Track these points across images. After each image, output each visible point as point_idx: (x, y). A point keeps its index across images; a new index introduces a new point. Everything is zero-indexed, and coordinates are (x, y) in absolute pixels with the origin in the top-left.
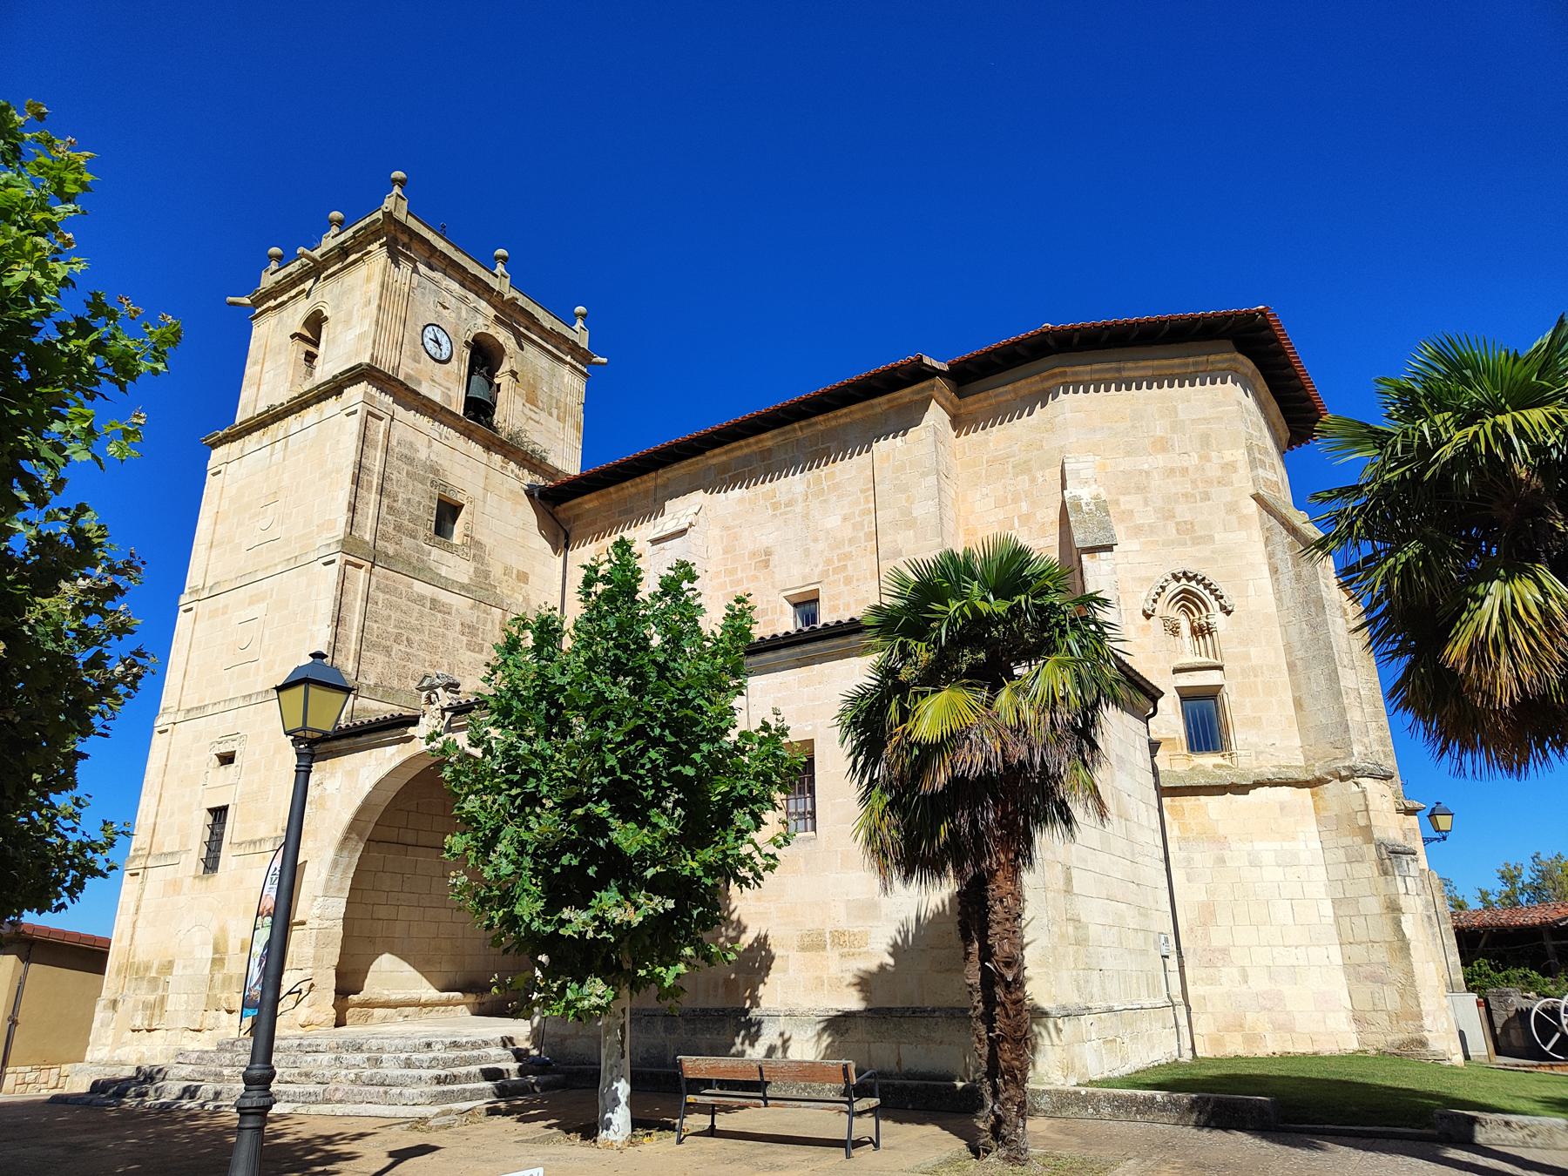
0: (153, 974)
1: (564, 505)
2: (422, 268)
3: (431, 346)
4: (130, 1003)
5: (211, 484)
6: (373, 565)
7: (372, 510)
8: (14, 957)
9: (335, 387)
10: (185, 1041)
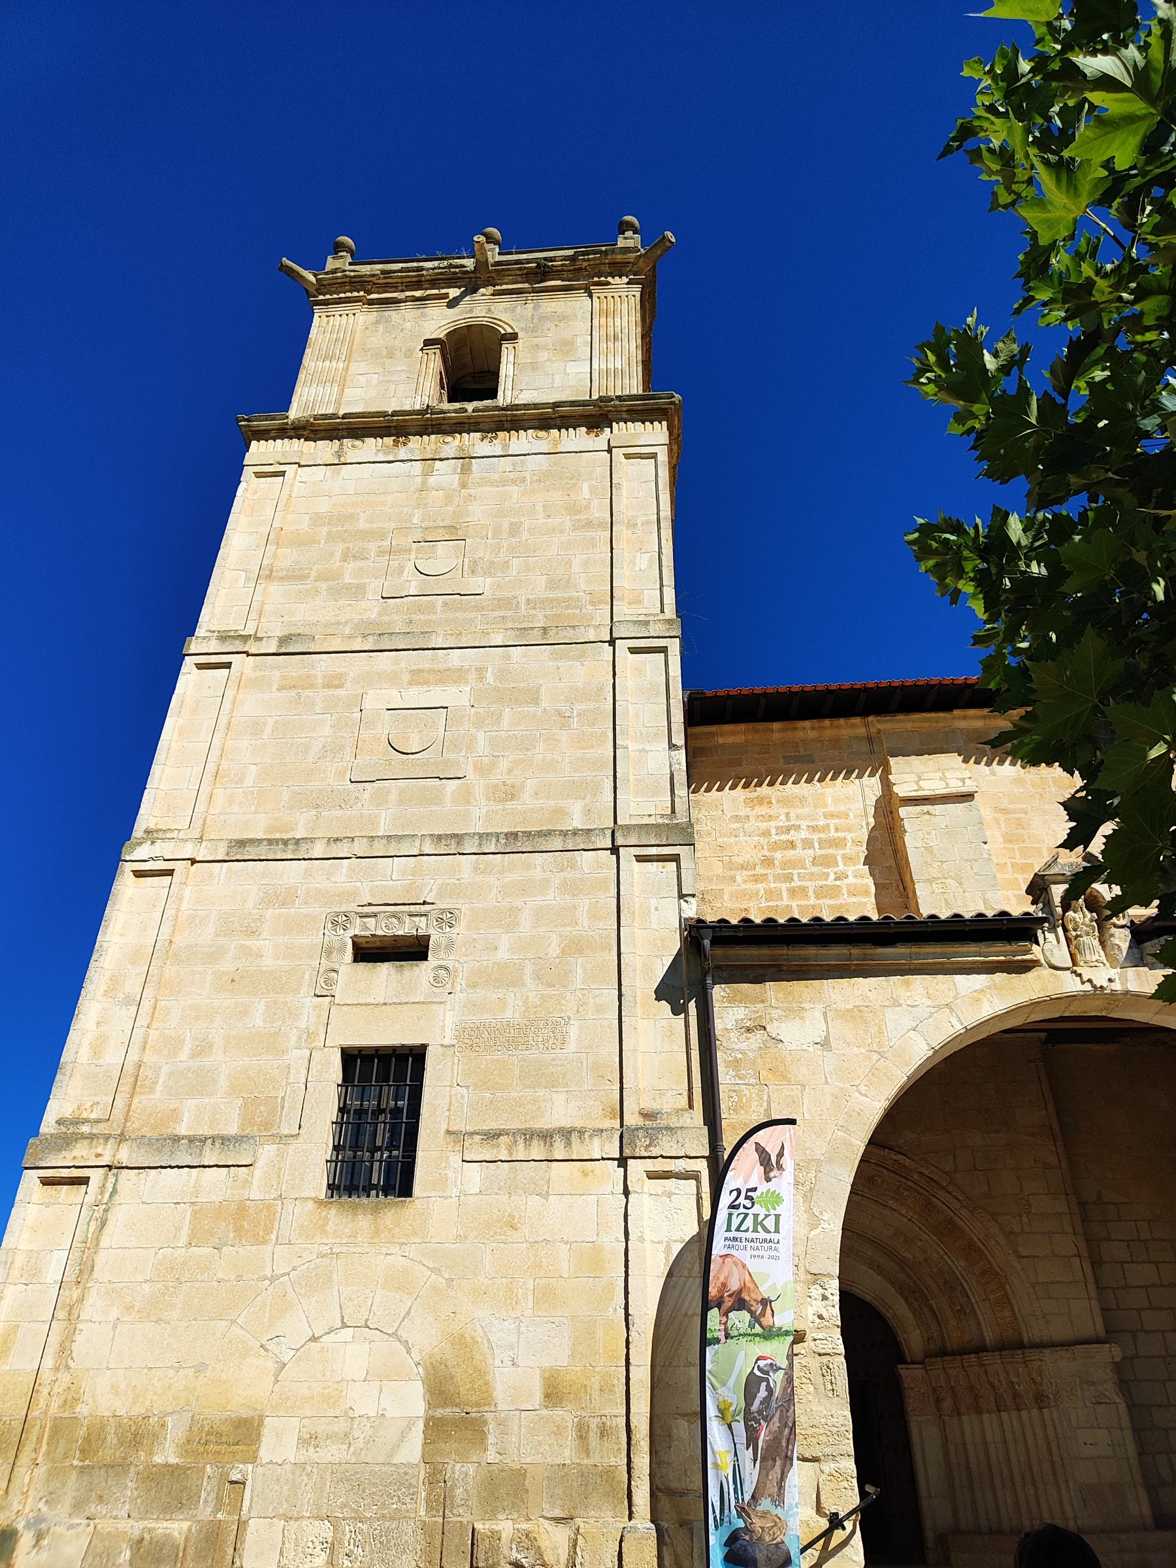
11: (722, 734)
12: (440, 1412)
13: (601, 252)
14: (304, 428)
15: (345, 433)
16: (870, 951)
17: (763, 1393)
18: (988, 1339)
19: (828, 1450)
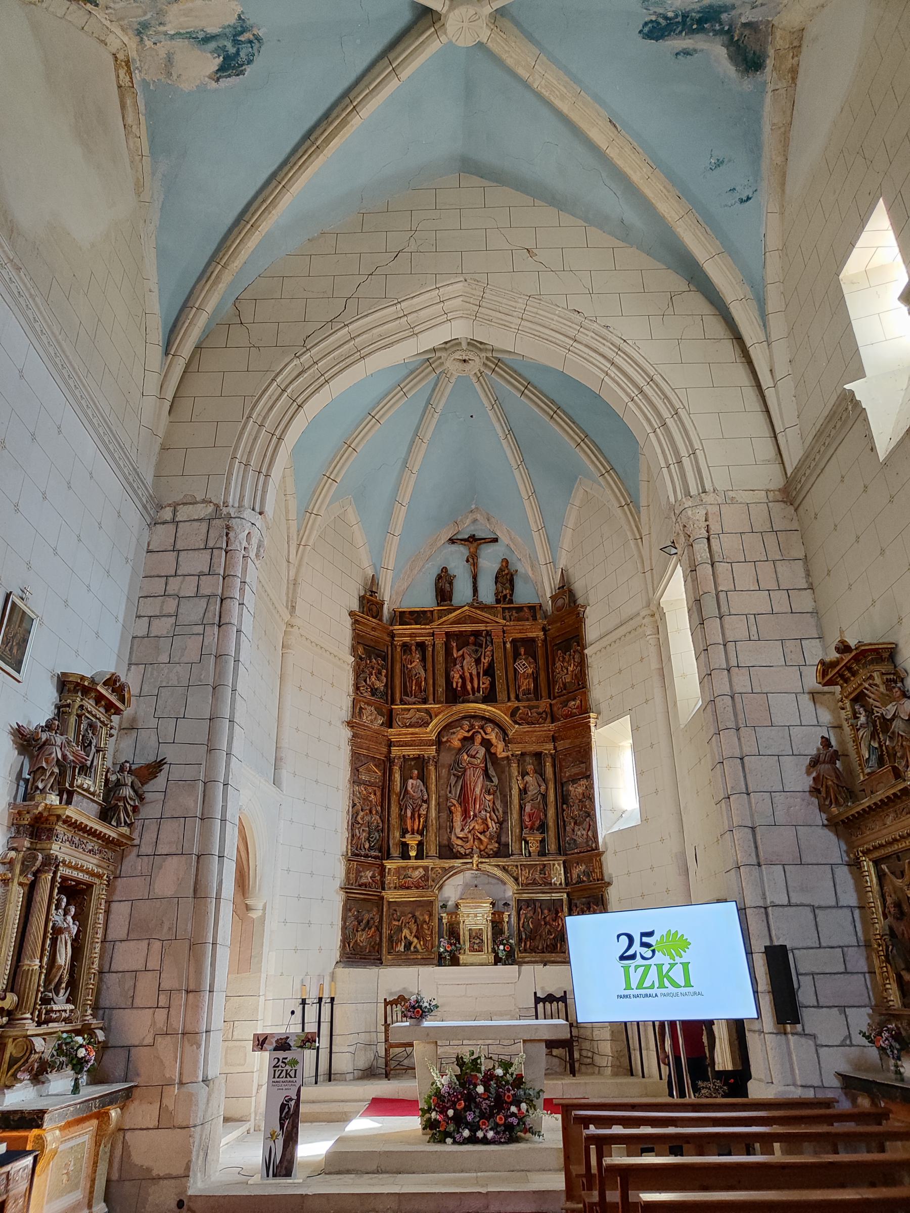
17: (286, 1110)
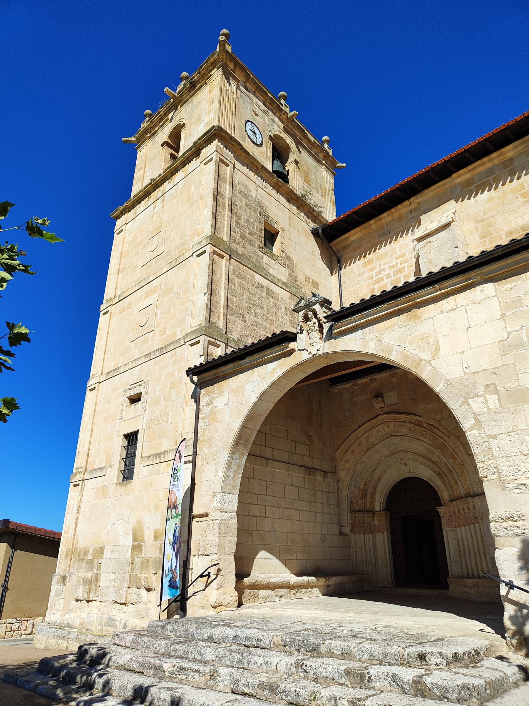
0: (90, 557)
1: (336, 241)
2: (242, 88)
3: (250, 133)
4: (74, 579)
5: (117, 239)
6: (231, 258)
7: (226, 221)
8: (5, 544)
9: (196, 151)
10: (114, 612)
11: (351, 236)
12: (135, 543)
13: (205, 63)
14: (126, 209)
15: (136, 204)
16: (239, 363)
18: (462, 493)
19: (211, 552)
